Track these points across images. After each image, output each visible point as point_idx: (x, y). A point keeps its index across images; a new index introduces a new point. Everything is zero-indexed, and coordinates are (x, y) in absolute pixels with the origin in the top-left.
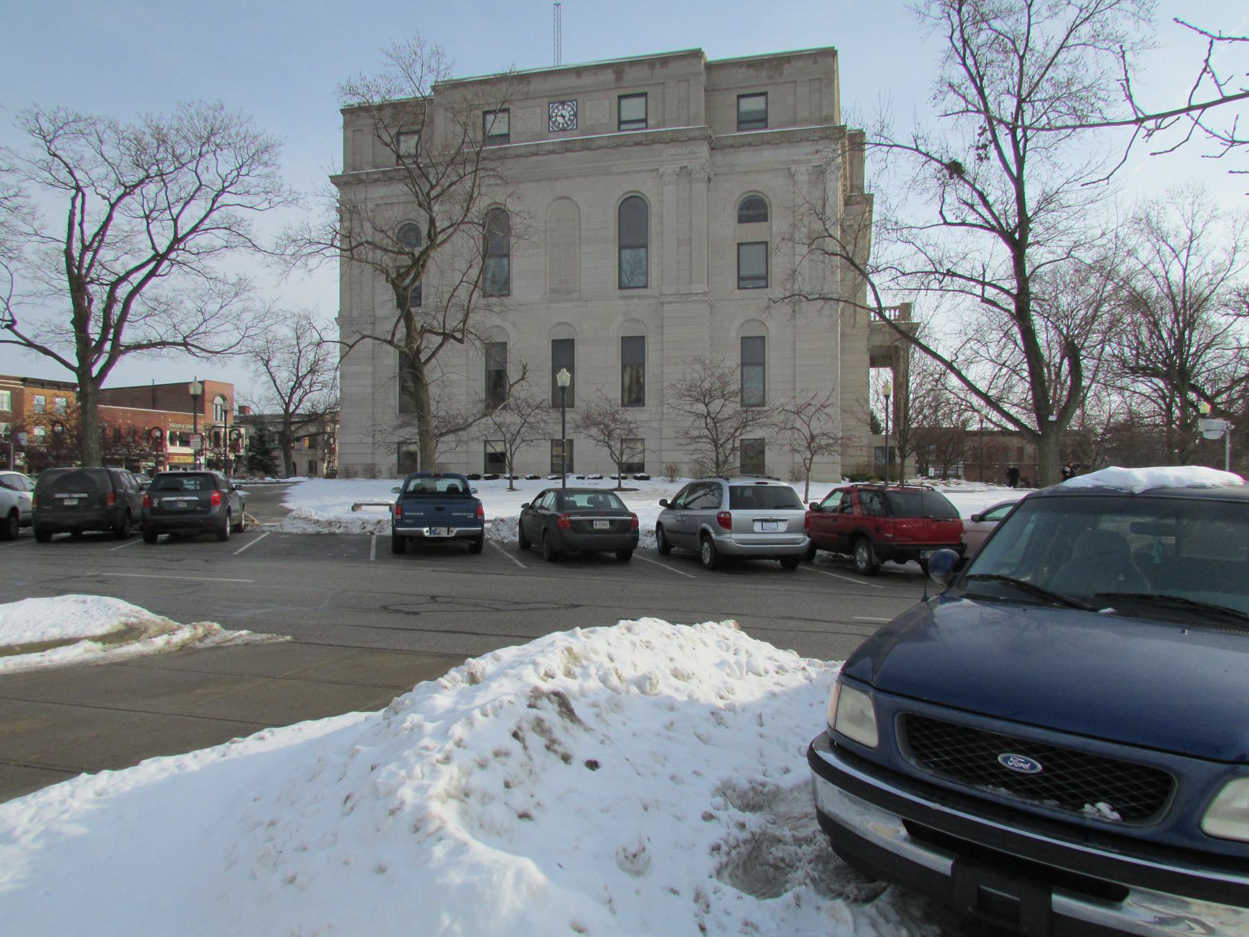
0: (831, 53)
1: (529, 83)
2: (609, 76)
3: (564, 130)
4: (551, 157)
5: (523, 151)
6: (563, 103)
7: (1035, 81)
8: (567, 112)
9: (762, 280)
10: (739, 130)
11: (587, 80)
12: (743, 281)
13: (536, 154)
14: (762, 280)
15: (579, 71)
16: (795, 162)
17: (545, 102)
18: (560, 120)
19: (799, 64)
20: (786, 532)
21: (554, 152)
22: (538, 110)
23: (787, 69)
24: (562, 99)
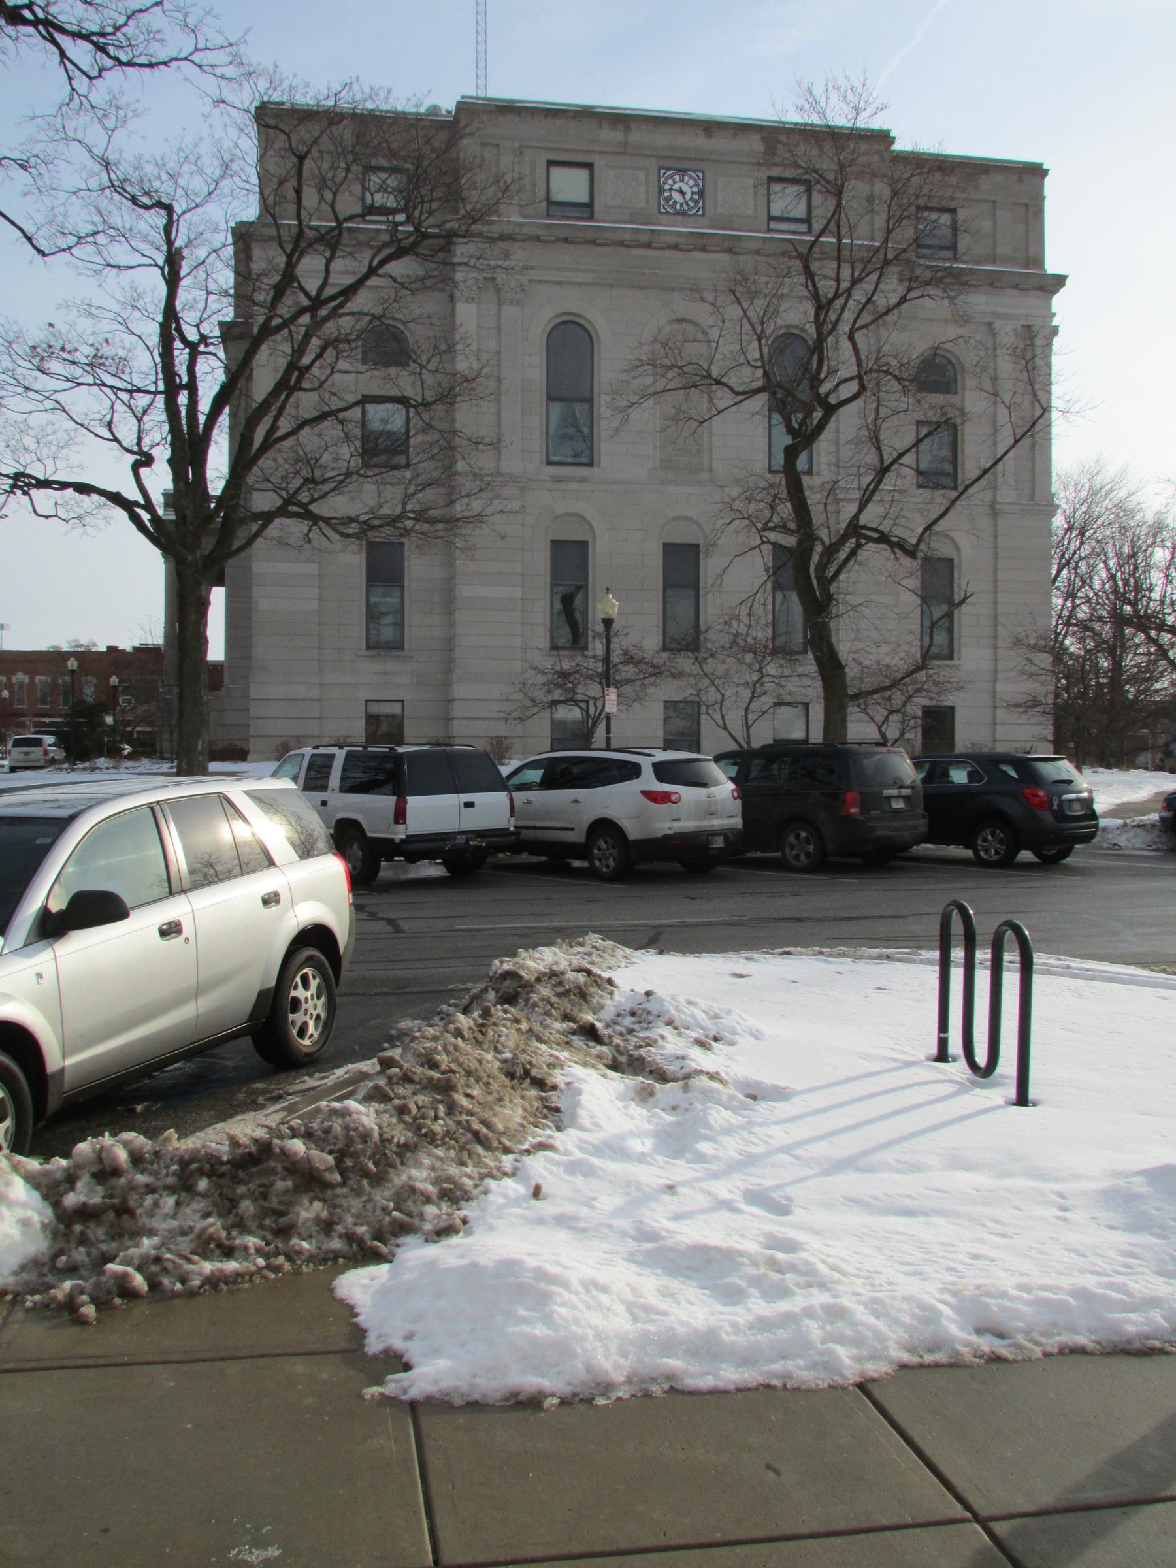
0: (1035, 173)
1: (627, 129)
2: (756, 144)
3: (682, 213)
4: (669, 254)
5: (627, 236)
6: (682, 172)
7: (136, 61)
8: (688, 185)
9: (397, 646)
10: (548, 215)
11: (721, 143)
12: (375, 646)
13: (648, 246)
14: (397, 646)
15: (710, 127)
16: (998, 316)
17: (653, 164)
18: (677, 196)
19: (999, 178)
20: (1141, 849)
21: (676, 247)
22: (641, 175)
23: (985, 183)
24: (680, 165)
